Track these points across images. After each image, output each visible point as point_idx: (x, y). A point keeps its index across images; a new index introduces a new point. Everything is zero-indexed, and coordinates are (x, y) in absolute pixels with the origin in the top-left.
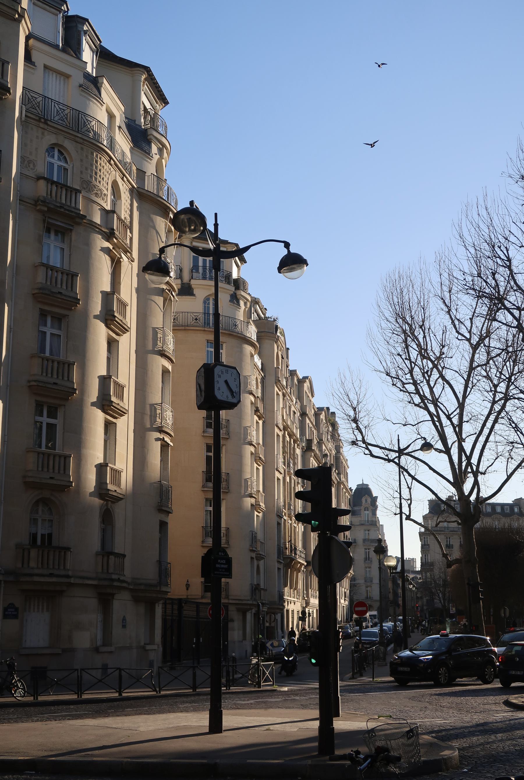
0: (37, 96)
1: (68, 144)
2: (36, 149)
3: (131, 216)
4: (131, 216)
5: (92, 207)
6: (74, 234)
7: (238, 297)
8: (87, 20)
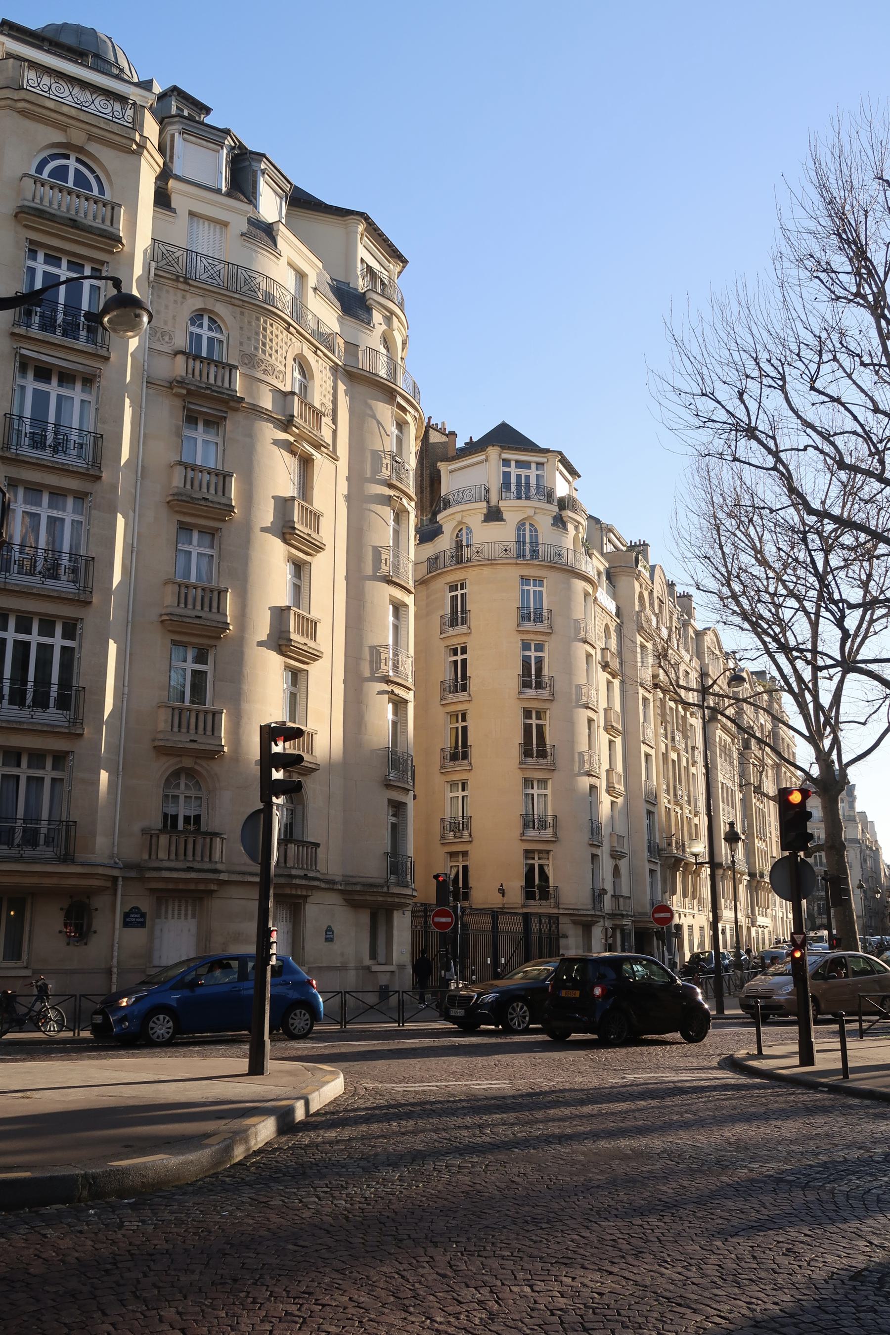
0: (175, 250)
1: (221, 309)
2: (174, 317)
3: (335, 402)
4: (335, 402)
5: (258, 388)
6: (229, 424)
7: (564, 519)
8: (264, 156)
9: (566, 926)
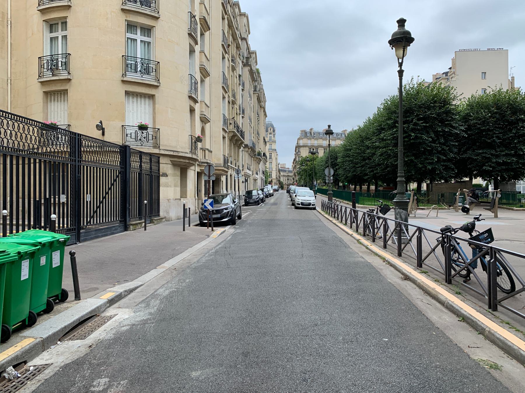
9: (165, 166)
